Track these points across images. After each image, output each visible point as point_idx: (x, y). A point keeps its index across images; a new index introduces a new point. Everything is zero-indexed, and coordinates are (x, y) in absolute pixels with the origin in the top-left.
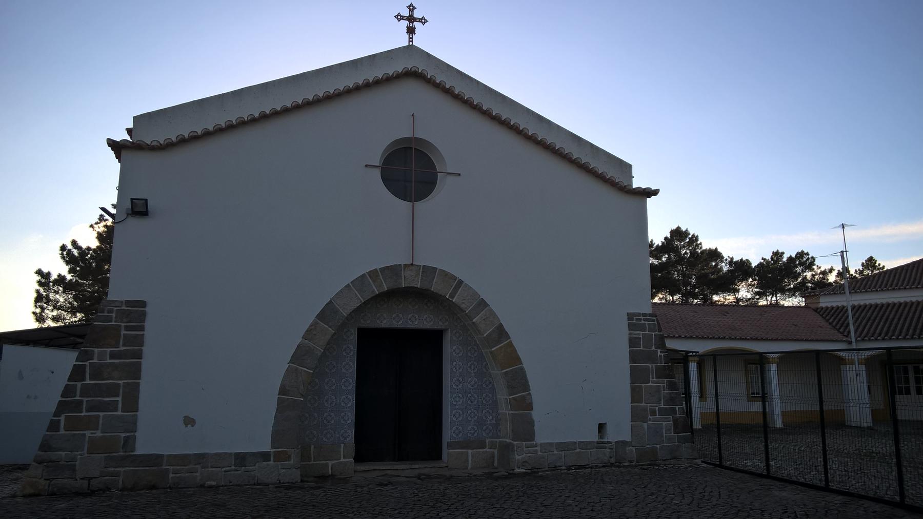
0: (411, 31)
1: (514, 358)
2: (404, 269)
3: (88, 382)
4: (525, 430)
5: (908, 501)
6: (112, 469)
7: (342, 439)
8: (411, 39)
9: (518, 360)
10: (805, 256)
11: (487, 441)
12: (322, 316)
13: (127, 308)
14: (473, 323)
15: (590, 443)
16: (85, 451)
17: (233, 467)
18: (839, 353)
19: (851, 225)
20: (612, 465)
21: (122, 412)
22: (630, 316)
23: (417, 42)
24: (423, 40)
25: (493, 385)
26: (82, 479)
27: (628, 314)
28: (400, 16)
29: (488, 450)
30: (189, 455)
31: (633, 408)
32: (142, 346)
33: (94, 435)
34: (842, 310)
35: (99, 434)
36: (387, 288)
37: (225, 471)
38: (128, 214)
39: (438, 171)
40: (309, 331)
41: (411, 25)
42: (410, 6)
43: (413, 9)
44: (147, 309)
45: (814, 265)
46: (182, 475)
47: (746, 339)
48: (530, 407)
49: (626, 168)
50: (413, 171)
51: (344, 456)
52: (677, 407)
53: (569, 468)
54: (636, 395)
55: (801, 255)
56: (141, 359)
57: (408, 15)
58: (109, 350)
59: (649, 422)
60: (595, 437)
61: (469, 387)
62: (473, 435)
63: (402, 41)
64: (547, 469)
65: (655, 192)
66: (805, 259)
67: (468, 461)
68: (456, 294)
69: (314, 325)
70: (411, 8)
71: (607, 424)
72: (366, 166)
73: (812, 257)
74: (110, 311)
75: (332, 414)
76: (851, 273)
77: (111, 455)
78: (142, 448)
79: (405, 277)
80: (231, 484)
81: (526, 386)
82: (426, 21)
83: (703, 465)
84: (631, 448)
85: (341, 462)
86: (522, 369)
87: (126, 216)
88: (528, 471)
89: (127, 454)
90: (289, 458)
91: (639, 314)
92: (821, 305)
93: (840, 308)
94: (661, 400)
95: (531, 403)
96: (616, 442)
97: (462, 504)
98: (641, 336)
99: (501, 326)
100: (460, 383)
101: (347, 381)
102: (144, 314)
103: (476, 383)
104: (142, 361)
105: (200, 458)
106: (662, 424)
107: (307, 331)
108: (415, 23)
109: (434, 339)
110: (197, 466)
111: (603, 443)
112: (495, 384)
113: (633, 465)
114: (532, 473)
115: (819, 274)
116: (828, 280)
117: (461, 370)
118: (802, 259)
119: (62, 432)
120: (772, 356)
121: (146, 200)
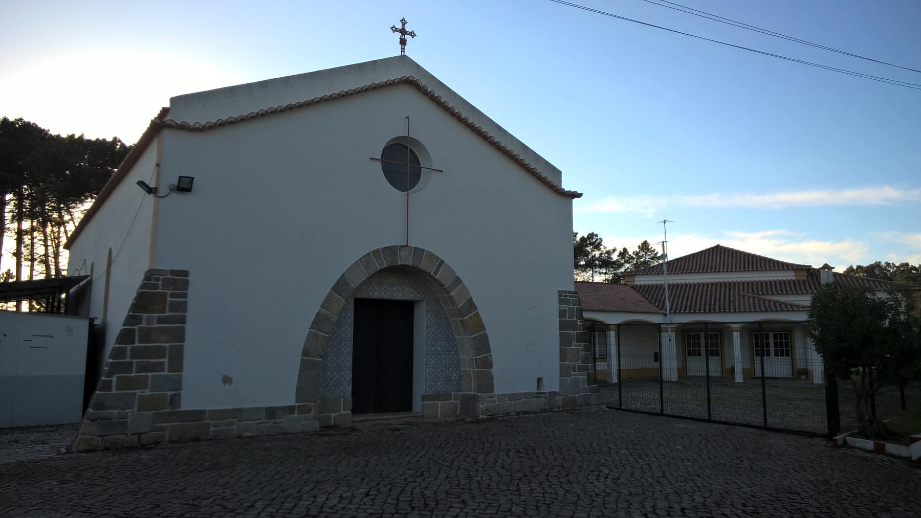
0: (403, 42)
1: (479, 325)
2: (400, 251)
3: (137, 344)
4: (486, 384)
5: (769, 425)
6: (160, 425)
7: (342, 394)
8: (403, 50)
9: (482, 327)
10: (595, 237)
11: (453, 393)
12: (336, 288)
13: (171, 277)
14: (451, 296)
15: (532, 393)
16: (136, 408)
17: (264, 420)
18: (731, 325)
19: (671, 221)
20: (546, 411)
21: (169, 371)
22: (560, 293)
23: (408, 53)
24: (413, 51)
25: (457, 348)
26: (133, 434)
27: (559, 291)
28: (395, 28)
29: (453, 402)
30: (228, 410)
31: (561, 366)
32: (185, 312)
33: (143, 394)
34: (660, 287)
35: (147, 392)
36: (387, 265)
37: (257, 424)
38: (171, 190)
39: (422, 166)
40: (326, 301)
41: (403, 37)
42: (402, 20)
43: (405, 23)
44: (189, 278)
45: (601, 245)
46: (221, 428)
47: (594, 311)
48: (490, 365)
49: (557, 173)
50: (408, 167)
51: (344, 408)
52: (590, 365)
53: (518, 414)
54: (563, 356)
55: (591, 236)
56: (185, 323)
57: (401, 28)
58: (156, 315)
59: (572, 377)
60: (534, 390)
61: (440, 349)
62: (442, 389)
63: (390, 49)
64: (502, 415)
65: (579, 195)
66: (594, 240)
67: (438, 411)
68: (439, 271)
69: (329, 296)
70: (404, 22)
71: (544, 378)
72: (371, 159)
73: (600, 239)
74: (157, 279)
75: (334, 373)
76: (630, 254)
77: (159, 411)
78: (186, 405)
79: (400, 257)
80: (263, 434)
81: (488, 350)
82: (415, 35)
83: (607, 409)
84: (559, 397)
85: (342, 415)
86: (486, 335)
87: (169, 191)
88: (488, 417)
89: (173, 410)
90: (310, 411)
91: (566, 292)
92: (636, 283)
93: (643, 287)
94: (579, 359)
95: (492, 362)
96: (549, 393)
97: (117, 489)
98: (567, 309)
99: (471, 299)
100: (433, 346)
101: (346, 344)
102: (187, 283)
103: (444, 346)
104: (186, 325)
105: (237, 413)
106: (579, 378)
107: (324, 301)
108: (406, 36)
109: (407, 308)
110: (234, 420)
111: (541, 393)
112: (459, 347)
113: (560, 411)
114: (492, 418)
115: (605, 254)
116: (612, 259)
117: (433, 335)
118: (592, 239)
119: (114, 391)
120: (733, 325)
121: (192, 178)
